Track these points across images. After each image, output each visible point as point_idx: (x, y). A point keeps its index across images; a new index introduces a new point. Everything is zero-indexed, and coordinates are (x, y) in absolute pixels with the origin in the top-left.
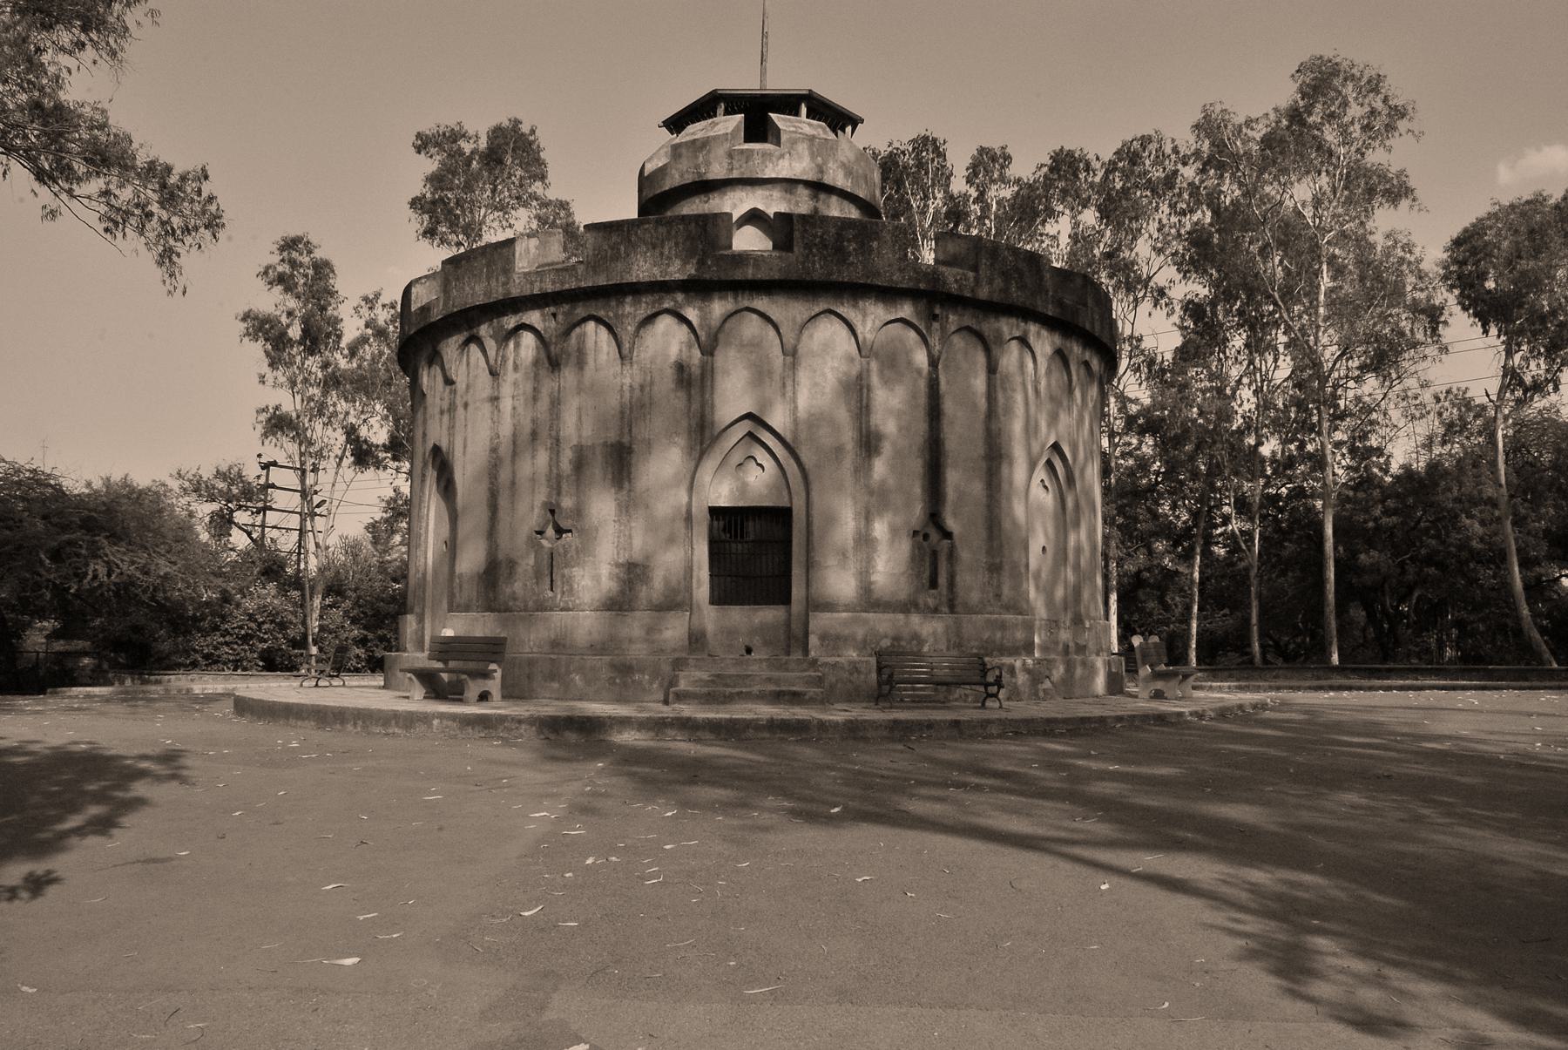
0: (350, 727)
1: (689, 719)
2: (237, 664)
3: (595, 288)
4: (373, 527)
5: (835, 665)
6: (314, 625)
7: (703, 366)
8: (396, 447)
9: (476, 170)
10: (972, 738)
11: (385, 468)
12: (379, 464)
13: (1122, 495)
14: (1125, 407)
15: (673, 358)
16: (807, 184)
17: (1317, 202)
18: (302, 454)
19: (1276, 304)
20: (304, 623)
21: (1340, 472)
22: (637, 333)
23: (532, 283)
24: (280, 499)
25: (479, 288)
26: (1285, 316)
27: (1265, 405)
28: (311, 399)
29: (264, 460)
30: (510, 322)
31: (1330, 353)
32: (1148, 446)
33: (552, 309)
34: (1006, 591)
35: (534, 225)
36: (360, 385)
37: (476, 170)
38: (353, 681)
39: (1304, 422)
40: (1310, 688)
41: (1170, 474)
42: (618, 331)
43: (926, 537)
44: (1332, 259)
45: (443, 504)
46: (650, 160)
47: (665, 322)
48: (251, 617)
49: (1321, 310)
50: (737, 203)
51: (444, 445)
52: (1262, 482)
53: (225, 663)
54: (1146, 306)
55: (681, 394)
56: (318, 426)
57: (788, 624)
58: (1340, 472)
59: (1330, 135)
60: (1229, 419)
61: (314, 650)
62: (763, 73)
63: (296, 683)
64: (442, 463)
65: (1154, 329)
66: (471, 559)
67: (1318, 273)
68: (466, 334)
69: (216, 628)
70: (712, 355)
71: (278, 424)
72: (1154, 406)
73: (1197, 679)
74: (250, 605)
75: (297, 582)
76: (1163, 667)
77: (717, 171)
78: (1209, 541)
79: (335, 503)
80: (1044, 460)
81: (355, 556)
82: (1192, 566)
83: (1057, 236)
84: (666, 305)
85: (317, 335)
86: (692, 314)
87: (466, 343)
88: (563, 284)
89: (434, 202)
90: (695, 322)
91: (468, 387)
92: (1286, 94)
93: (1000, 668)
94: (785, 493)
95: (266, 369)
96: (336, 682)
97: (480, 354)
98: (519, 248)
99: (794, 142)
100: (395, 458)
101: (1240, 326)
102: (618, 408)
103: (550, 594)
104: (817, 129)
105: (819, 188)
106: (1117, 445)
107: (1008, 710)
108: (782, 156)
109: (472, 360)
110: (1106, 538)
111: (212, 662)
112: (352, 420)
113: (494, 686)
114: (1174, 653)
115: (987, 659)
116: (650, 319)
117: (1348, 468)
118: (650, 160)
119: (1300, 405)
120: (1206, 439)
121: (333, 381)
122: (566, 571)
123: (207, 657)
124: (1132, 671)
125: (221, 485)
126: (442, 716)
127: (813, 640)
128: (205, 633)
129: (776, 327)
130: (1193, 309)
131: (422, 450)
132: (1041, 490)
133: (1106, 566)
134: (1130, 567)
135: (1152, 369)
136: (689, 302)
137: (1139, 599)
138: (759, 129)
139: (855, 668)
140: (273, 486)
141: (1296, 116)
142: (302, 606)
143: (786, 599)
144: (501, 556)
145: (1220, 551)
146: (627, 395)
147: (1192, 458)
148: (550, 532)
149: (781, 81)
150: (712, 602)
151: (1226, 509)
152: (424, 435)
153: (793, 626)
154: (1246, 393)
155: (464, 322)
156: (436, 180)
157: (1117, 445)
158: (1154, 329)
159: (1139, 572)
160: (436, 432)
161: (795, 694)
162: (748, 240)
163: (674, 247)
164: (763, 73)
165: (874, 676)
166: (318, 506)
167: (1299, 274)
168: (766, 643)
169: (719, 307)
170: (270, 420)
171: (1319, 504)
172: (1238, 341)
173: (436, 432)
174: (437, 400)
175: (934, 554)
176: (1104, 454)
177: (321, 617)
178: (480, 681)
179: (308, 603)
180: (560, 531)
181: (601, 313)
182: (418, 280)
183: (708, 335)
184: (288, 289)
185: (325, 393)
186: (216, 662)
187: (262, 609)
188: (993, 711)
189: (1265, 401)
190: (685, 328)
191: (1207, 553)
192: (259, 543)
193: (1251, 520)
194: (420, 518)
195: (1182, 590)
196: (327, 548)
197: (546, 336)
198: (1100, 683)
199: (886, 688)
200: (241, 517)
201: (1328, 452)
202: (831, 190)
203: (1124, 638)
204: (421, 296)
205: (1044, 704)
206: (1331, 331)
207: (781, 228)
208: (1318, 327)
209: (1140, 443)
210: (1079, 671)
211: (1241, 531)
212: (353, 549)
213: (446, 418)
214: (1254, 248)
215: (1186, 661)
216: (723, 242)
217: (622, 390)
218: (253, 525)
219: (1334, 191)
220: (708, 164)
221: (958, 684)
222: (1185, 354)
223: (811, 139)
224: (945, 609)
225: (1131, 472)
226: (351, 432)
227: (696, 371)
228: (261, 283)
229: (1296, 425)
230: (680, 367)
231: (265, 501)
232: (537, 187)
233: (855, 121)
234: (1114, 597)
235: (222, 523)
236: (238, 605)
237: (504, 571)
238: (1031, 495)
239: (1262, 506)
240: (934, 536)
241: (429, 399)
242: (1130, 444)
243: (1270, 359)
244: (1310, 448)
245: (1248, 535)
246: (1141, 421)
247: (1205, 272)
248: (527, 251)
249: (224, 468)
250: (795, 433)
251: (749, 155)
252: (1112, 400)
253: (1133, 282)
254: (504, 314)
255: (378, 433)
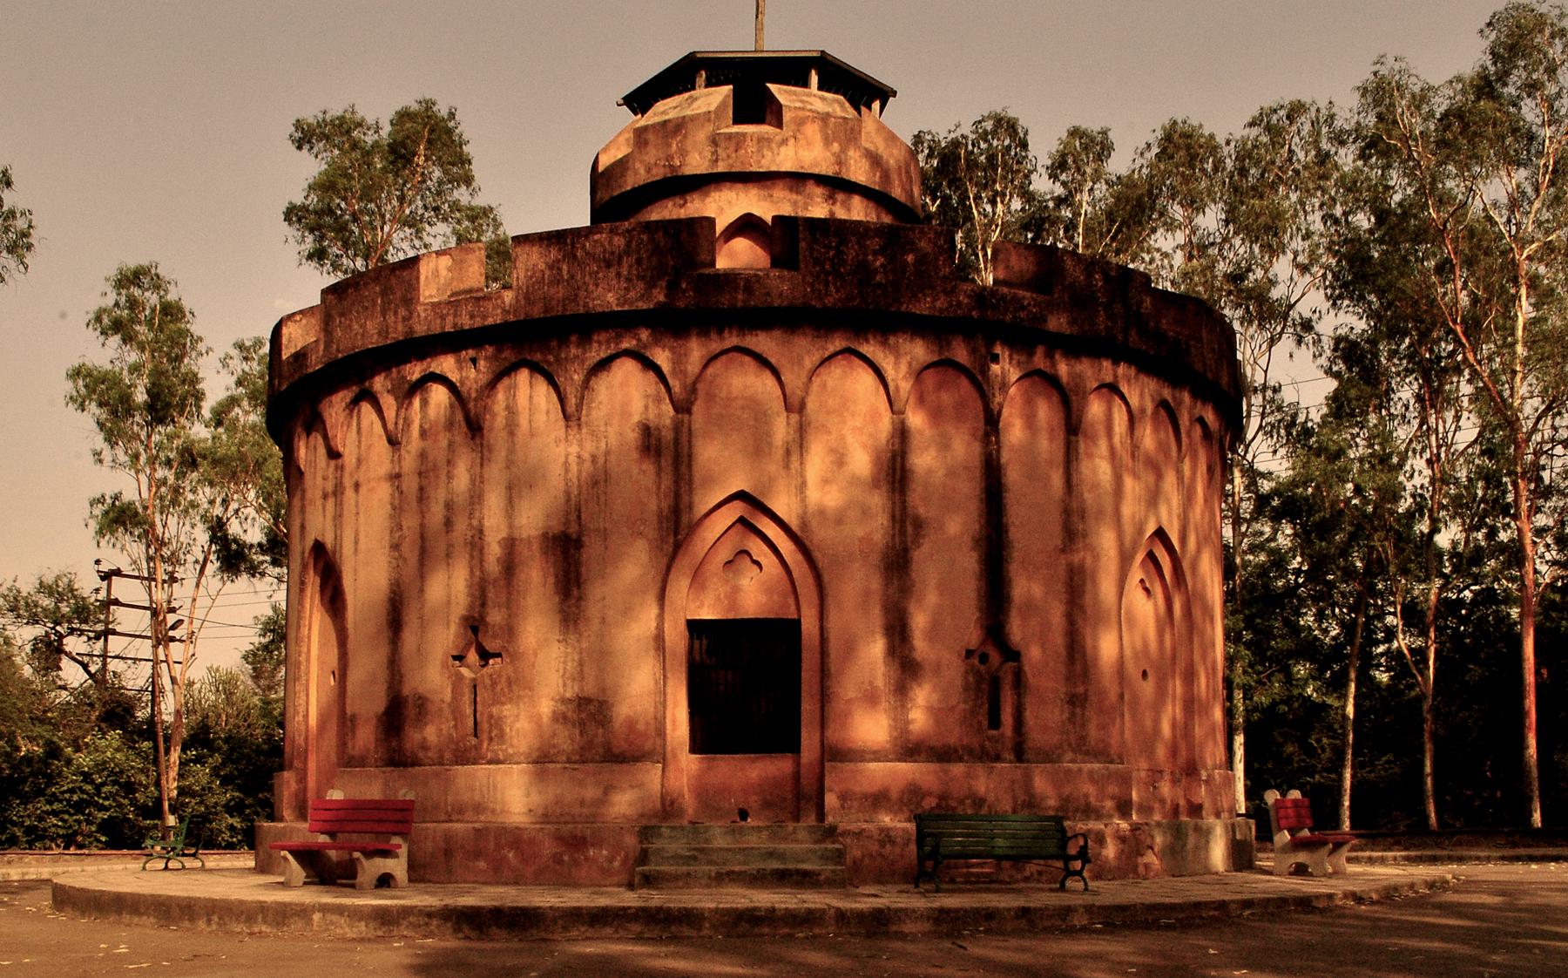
0: (202, 924)
1: (660, 909)
2: (70, 841)
3: (539, 335)
4: (251, 657)
5: (859, 834)
6: (171, 787)
7: (677, 427)
8: (276, 547)
9: (380, 169)
10: (1049, 931)
11: (263, 574)
12: (254, 570)
13: (1246, 604)
14: (1254, 483)
15: (636, 418)
16: (821, 180)
17: (1514, 204)
18: (150, 559)
19: (1457, 341)
20: (158, 784)
21: (1543, 568)
22: (586, 384)
23: (443, 318)
24: (125, 619)
25: (372, 326)
26: (1470, 357)
27: (1441, 479)
28: (164, 482)
29: (104, 567)
30: (415, 371)
31: (1530, 407)
32: (1285, 536)
33: (471, 353)
34: (1093, 732)
35: (453, 243)
36: (230, 469)
37: (380, 169)
38: (213, 860)
39: (1496, 501)
40: (1503, 858)
41: (1314, 575)
42: (561, 381)
43: (984, 658)
44: (1534, 282)
45: (328, 620)
46: (605, 150)
47: (626, 370)
48: (87, 777)
49: (1520, 349)
50: (724, 207)
51: (329, 541)
52: (1438, 582)
53: (52, 840)
54: (1287, 343)
55: (649, 467)
56: (172, 521)
57: (797, 776)
58: (1543, 568)
59: (1530, 112)
60: (1396, 498)
61: (171, 820)
62: (759, 29)
63: (135, 865)
64: (326, 565)
65: (1295, 376)
66: (369, 702)
67: (1515, 298)
68: (355, 389)
69: (40, 792)
70: (689, 411)
71: (119, 518)
72: (1293, 483)
73: (1353, 849)
74: (84, 760)
75: (150, 729)
76: (1306, 833)
77: (697, 163)
78: (1368, 662)
79: (197, 624)
80: (1140, 556)
81: (229, 695)
82: (1344, 697)
83: (1164, 255)
84: (625, 345)
85: (168, 402)
86: (662, 358)
87: (355, 402)
88: (485, 317)
89: (319, 213)
90: (666, 367)
91: (359, 462)
92: (1469, 55)
93: (1085, 836)
94: (791, 601)
95: (99, 441)
96: (190, 863)
97: (374, 417)
98: (425, 269)
99: (800, 123)
100: (275, 563)
101: (1408, 372)
102: (562, 487)
103: (474, 741)
104: (835, 105)
105: (836, 185)
106: (1244, 535)
107: (1096, 893)
108: (784, 142)
109: (365, 423)
110: (1230, 660)
111: (36, 838)
112: (218, 511)
113: (397, 867)
114: (1322, 812)
115: (1067, 823)
116: (604, 365)
117: (1554, 563)
118: (605, 150)
119: (1492, 479)
120: (1364, 525)
121: (189, 459)
122: (494, 710)
123: (30, 830)
124: (1265, 835)
125: (47, 602)
126: (325, 909)
127: (831, 800)
128: (26, 799)
129: (776, 373)
130: (1347, 349)
131: (299, 548)
132: (1140, 595)
133: (1230, 697)
134: (1262, 699)
135: (1295, 433)
136: (657, 341)
137: (1279, 744)
138: (754, 105)
139: (887, 836)
140: (117, 602)
141: (1485, 87)
142: (156, 762)
143: (791, 745)
144: (406, 690)
145: (1383, 677)
146: (574, 468)
147: (1344, 552)
148: (473, 657)
149: (781, 41)
150: (693, 750)
151: (1390, 620)
152: (303, 527)
153: (804, 782)
154: (1419, 463)
155: (353, 372)
156: (325, 186)
157: (1244, 535)
158: (1295, 376)
159: (1274, 704)
160: (318, 524)
161: (806, 874)
162: (738, 255)
163: (643, 273)
164: (759, 29)
165: (913, 847)
166: (173, 628)
167: (1488, 301)
168: (767, 804)
169: (696, 351)
170: (107, 512)
171: (1515, 612)
172: (1406, 393)
173: (318, 524)
174: (319, 480)
175: (995, 684)
176: (1226, 547)
177: (181, 776)
178: (379, 861)
179: (162, 758)
180: (485, 656)
181: (538, 357)
182: (290, 317)
183: (684, 386)
184: (127, 339)
185: (180, 475)
186: (41, 838)
187: (101, 766)
188: (1077, 893)
189: (1443, 472)
190: (651, 375)
191: (1365, 680)
192: (99, 679)
193: (1424, 633)
194: (298, 640)
195: (1330, 728)
196: (191, 684)
197: (464, 390)
198: (1218, 854)
199: (929, 864)
200: (74, 644)
201: (1528, 541)
202: (850, 188)
203: (1253, 793)
204: (297, 338)
205: (1145, 883)
206: (1531, 379)
207: (781, 237)
208: (1514, 372)
209: (1275, 531)
210: (1191, 841)
211: (1410, 650)
212: (226, 685)
213: (331, 502)
214: (1431, 264)
215: (1337, 823)
216: (704, 257)
217: (566, 463)
218: (91, 655)
219: (1537, 190)
220: (683, 153)
221: (1028, 858)
222: (1340, 408)
223: (825, 118)
224: (1008, 756)
225: (1263, 571)
226: (217, 529)
227: (668, 435)
228: (93, 335)
229: (1486, 502)
230: (646, 430)
231: (107, 623)
232: (462, 195)
233: (883, 94)
234: (1239, 740)
235: (49, 652)
236: (69, 762)
237: (411, 711)
238: (1130, 620)
239: (1438, 614)
240: (995, 657)
241: (308, 477)
242: (1262, 533)
243: (1449, 415)
244: (1503, 536)
245: (1420, 653)
246: (1275, 503)
247: (1362, 298)
248: (436, 273)
249: (49, 579)
250: (804, 525)
251: (739, 141)
252: (1237, 474)
253: (1269, 312)
254: (406, 362)
255: (251, 529)
